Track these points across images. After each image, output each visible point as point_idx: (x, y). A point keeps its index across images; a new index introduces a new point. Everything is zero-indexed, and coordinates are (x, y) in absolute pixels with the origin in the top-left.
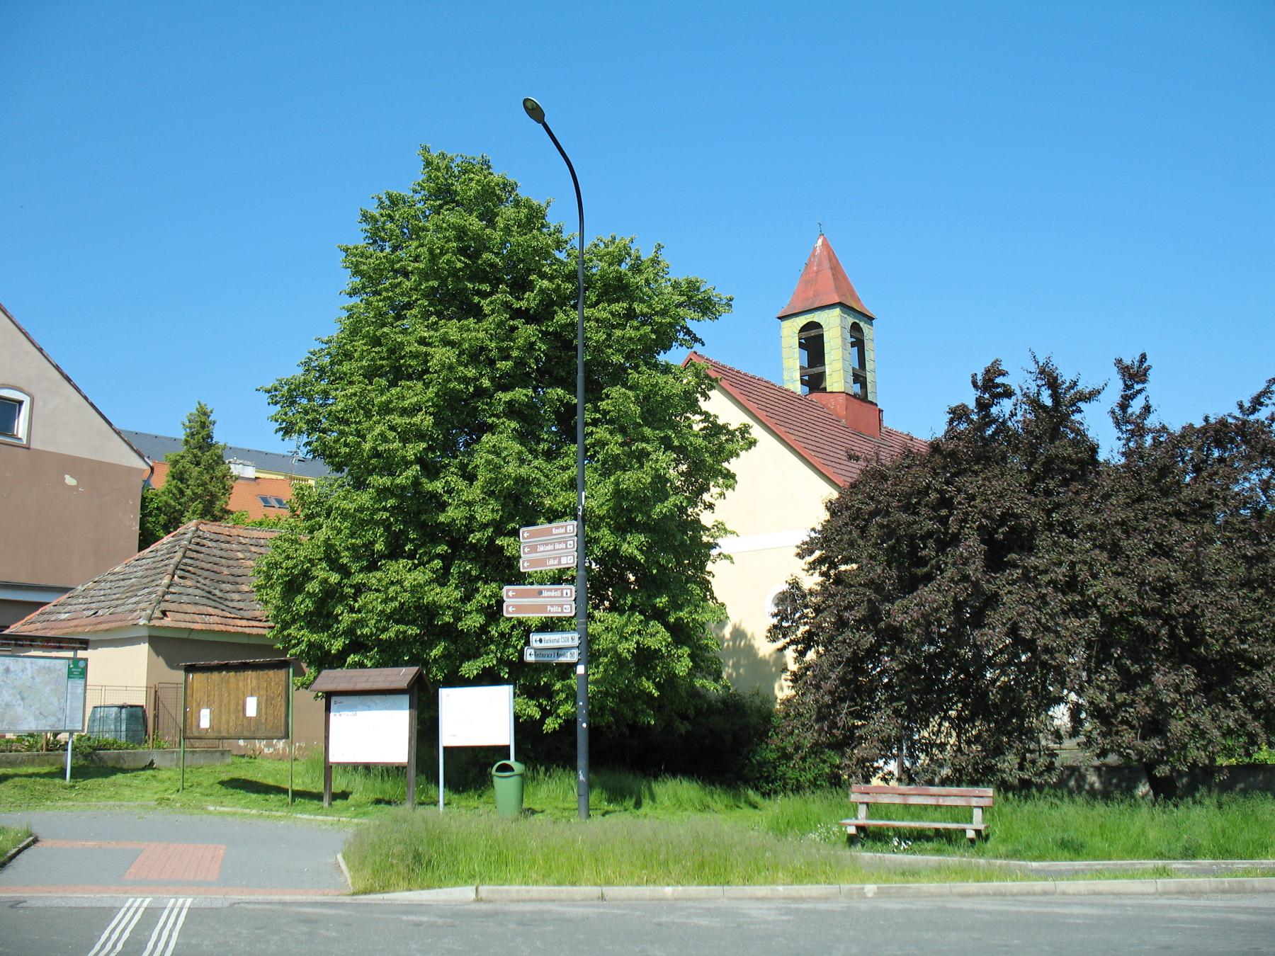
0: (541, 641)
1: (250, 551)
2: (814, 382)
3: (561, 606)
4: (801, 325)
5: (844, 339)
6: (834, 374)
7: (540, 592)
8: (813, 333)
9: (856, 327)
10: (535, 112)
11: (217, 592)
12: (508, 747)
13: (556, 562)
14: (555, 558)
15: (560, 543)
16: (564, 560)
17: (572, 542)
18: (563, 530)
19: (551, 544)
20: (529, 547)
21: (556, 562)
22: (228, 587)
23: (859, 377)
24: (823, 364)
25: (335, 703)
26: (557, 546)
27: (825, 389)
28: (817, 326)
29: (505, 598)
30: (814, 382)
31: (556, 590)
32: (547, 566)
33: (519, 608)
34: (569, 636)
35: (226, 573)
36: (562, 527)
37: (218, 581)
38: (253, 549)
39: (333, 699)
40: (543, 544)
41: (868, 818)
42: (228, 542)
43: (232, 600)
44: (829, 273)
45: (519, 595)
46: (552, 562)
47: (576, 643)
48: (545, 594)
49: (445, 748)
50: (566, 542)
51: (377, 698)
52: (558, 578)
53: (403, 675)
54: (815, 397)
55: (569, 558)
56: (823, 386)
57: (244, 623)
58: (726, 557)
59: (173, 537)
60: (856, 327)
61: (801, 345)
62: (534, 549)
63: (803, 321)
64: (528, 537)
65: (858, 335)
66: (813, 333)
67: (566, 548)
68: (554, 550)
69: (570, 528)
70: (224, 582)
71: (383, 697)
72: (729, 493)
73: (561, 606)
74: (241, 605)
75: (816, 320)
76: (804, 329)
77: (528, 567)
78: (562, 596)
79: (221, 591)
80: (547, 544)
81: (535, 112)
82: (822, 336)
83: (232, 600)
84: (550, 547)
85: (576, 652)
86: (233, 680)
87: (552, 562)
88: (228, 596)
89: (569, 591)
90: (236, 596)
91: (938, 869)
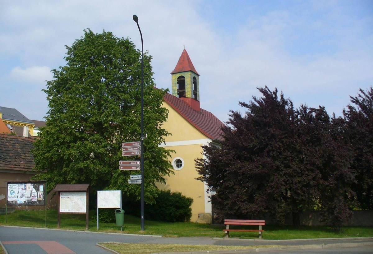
0: (133, 178)
1: (10, 143)
2: (182, 93)
3: (136, 167)
4: (178, 77)
5: (191, 82)
6: (188, 92)
7: (130, 163)
8: (182, 79)
9: (194, 78)
10: (135, 18)
11: (3, 156)
13: (134, 153)
14: (133, 152)
15: (135, 148)
16: (136, 153)
17: (139, 148)
19: (132, 148)
21: (134, 153)
22: (5, 154)
23: (195, 93)
24: (185, 89)
25: (61, 194)
26: (134, 149)
27: (185, 96)
28: (183, 77)
29: (120, 164)
30: (182, 93)
31: (135, 162)
32: (130, 155)
33: (124, 167)
34: (139, 176)
35: (4, 150)
37: (2, 153)
38: (11, 142)
39: (60, 193)
42: (3, 140)
43: (7, 159)
44: (187, 61)
45: (124, 163)
46: (132, 153)
47: (141, 178)
48: (132, 163)
49: (99, 209)
51: (76, 193)
52: (136, 158)
53: (85, 187)
54: (182, 98)
56: (184, 95)
57: (12, 166)
60: (194, 78)
61: (178, 83)
62: (126, 149)
63: (179, 75)
64: (125, 146)
65: (195, 80)
66: (182, 79)
67: (137, 149)
68: (133, 150)
69: (138, 144)
70: (4, 153)
71: (77, 193)
73: (136, 167)
74: (10, 160)
75: (183, 75)
76: (179, 78)
78: (137, 164)
79: (3, 156)
80: (131, 148)
81: (135, 18)
82: (184, 80)
83: (7, 159)
84: (132, 149)
85: (141, 180)
86: (75, 198)
87: (132, 153)
88: (6, 157)
89: (139, 162)
90: (8, 157)
91: (262, 247)
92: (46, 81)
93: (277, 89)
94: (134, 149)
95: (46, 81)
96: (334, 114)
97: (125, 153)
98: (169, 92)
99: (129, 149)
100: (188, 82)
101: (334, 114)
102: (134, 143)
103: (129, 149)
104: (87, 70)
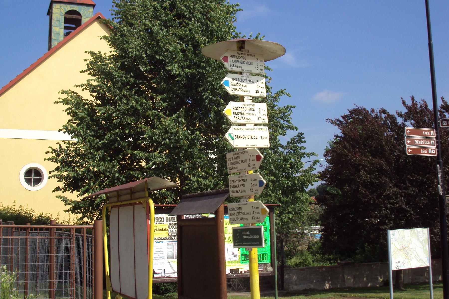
4: (67, 10)
8: (74, 17)
12: (428, 267)
14: (425, 149)
15: (427, 140)
16: (430, 151)
18: (428, 133)
19: (422, 140)
20: (410, 140)
26: (426, 143)
28: (78, 14)
36: (428, 131)
39: (135, 206)
40: (418, 139)
41: (229, 163)
46: (423, 151)
50: (430, 141)
55: (433, 150)
58: (84, 71)
59: (239, 205)
66: (74, 17)
72: (283, 89)
76: (68, 13)
77: (411, 153)
80: (420, 140)
84: (421, 142)
87: (423, 151)
92: (59, 92)
93: (404, 100)
94: (426, 143)
95: (59, 92)
96: (413, 99)
97: (411, 149)
98: (66, 201)
99: (417, 142)
100: (164, 234)
101: (413, 99)
102: (426, 131)
103: (417, 142)
104: (168, 84)
